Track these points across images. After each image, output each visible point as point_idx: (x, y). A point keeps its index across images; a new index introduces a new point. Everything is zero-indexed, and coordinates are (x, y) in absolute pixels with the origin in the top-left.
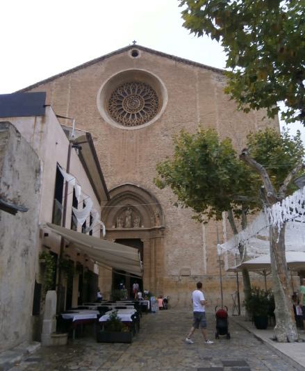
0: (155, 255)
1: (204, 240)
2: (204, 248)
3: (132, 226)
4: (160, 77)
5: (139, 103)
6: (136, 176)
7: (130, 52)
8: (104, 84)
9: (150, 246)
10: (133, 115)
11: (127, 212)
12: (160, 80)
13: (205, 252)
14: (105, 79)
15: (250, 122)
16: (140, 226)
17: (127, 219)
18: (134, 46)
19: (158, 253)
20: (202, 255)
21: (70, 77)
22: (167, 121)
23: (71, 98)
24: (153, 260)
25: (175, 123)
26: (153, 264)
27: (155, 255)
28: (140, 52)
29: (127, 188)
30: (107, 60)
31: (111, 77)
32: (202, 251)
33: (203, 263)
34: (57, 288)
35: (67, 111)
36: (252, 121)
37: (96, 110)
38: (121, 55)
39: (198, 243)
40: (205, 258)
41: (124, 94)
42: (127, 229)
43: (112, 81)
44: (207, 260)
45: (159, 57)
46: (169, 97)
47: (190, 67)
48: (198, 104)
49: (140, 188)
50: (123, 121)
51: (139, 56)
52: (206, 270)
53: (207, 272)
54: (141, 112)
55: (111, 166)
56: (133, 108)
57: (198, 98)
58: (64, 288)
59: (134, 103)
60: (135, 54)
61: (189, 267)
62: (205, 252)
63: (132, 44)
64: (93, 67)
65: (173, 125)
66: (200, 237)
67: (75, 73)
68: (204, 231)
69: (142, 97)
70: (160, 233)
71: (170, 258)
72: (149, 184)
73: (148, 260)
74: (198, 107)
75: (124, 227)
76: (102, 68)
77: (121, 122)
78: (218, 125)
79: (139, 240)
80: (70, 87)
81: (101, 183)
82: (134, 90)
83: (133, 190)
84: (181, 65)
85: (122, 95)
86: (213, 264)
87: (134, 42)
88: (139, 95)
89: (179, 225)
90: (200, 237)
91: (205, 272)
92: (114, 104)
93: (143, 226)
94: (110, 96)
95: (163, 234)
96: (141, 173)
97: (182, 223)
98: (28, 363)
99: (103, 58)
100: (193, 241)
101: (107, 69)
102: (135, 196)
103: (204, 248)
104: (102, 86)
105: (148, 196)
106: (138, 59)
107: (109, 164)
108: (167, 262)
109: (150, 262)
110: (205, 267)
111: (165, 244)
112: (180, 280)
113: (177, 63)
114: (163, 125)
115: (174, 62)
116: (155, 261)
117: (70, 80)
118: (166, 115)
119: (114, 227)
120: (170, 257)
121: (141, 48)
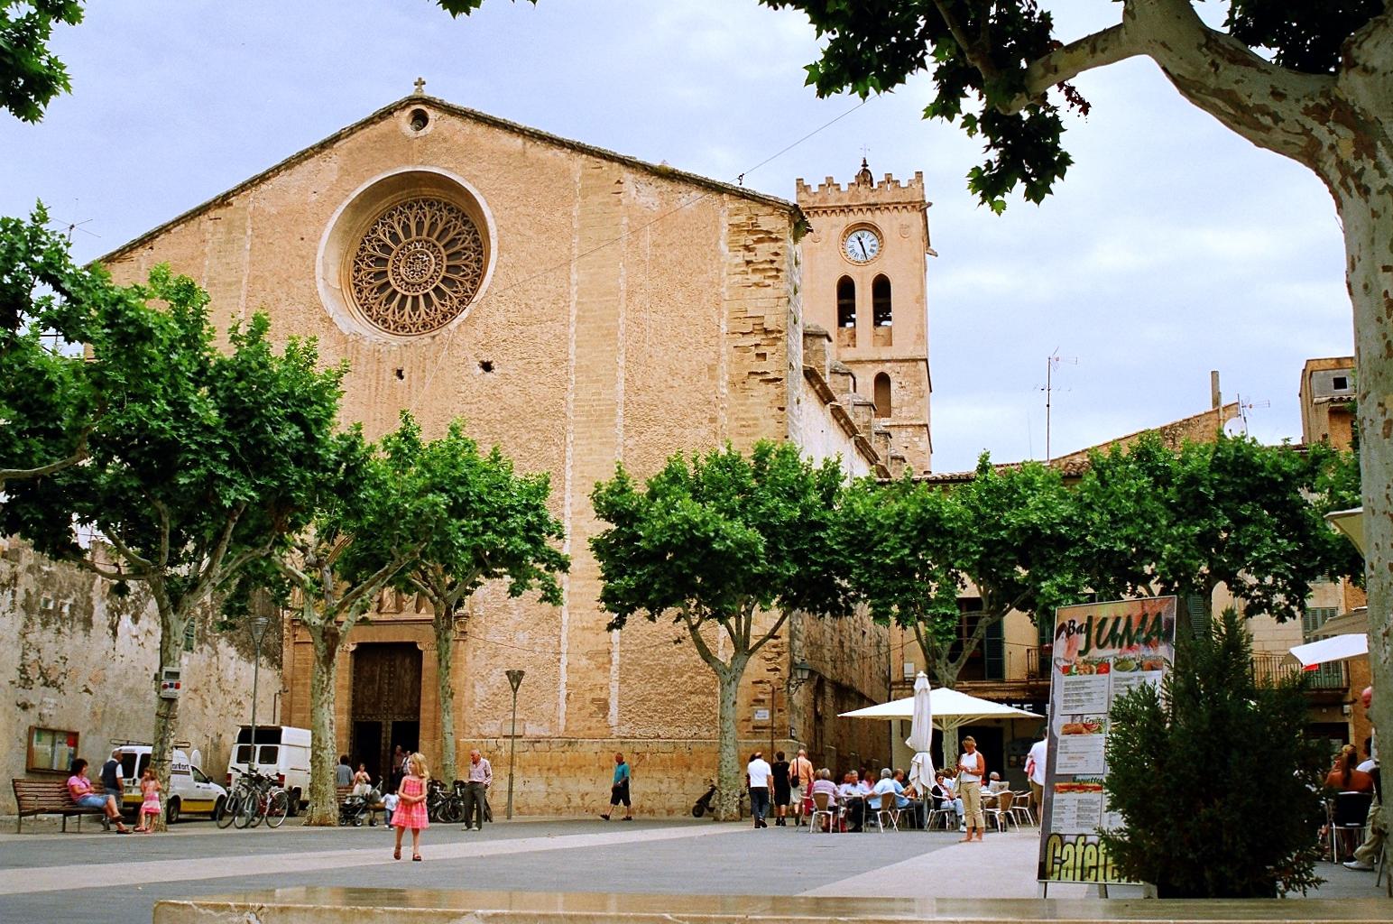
1: (564, 649)
2: (563, 667)
3: (399, 609)
5: (433, 265)
7: (403, 119)
8: (335, 217)
10: (416, 299)
13: (564, 679)
14: (336, 204)
15: (708, 319)
16: (418, 611)
20: (556, 684)
22: (490, 322)
23: (252, 263)
25: (511, 325)
28: (432, 114)
31: (354, 195)
34: (1374, 752)
35: (242, 303)
36: (713, 311)
38: (383, 126)
40: (564, 692)
41: (385, 248)
42: (389, 617)
47: (562, 154)
48: (573, 269)
50: (390, 318)
51: (429, 128)
52: (562, 722)
54: (437, 289)
56: (417, 279)
58: (1375, 747)
59: (418, 267)
63: (410, 91)
64: (309, 165)
65: (505, 334)
66: (554, 641)
67: (263, 187)
68: (565, 622)
72: (130, 617)
74: (574, 277)
75: (378, 611)
76: (330, 165)
77: (385, 321)
78: (622, 328)
82: (406, 229)
84: (539, 151)
85: (388, 242)
87: (420, 83)
88: (433, 239)
90: (554, 641)
91: (562, 728)
92: (369, 269)
93: (423, 611)
94: (357, 248)
101: (344, 171)
103: (563, 667)
104: (331, 224)
106: (425, 139)
108: (472, 704)
112: (499, 747)
113: (529, 144)
115: (519, 142)
118: (488, 305)
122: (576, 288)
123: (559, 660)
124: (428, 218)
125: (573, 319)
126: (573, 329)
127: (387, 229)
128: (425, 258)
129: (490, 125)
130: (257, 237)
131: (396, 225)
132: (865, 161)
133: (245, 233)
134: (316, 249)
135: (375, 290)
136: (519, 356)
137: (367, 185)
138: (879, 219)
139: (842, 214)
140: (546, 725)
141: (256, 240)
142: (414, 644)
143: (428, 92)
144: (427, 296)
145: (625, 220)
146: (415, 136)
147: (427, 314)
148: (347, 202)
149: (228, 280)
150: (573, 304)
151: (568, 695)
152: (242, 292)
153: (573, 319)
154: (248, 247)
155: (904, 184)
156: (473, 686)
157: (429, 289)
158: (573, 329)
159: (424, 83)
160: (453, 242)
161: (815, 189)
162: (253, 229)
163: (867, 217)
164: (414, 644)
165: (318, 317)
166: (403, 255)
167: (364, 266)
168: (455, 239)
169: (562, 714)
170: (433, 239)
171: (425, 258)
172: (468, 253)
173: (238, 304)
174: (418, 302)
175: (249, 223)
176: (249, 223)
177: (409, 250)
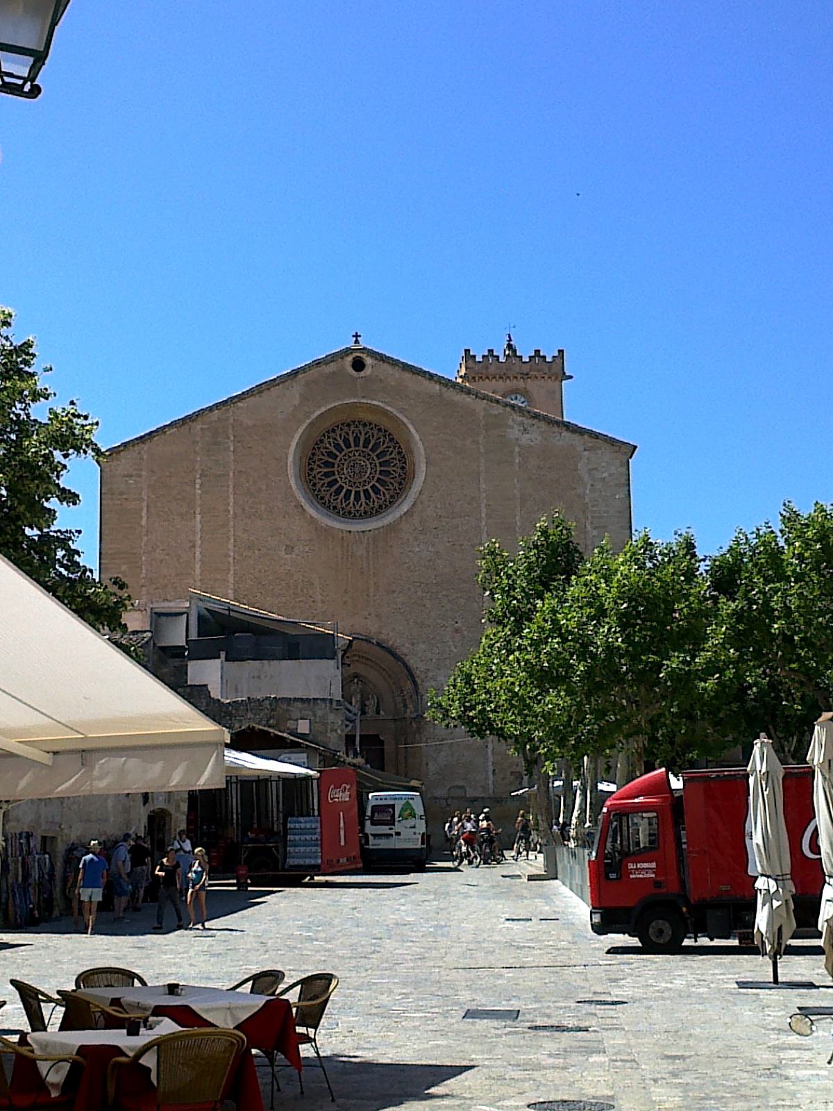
8: (301, 431)
13: (491, 759)
14: (300, 422)
28: (368, 361)
33: (487, 778)
38: (332, 367)
40: (491, 768)
50: (339, 506)
51: (367, 371)
52: (491, 786)
53: (493, 792)
57: (482, 468)
60: (358, 365)
62: (491, 759)
69: (373, 455)
71: (432, 767)
76: (295, 390)
91: (491, 791)
101: (304, 398)
113: (444, 389)
122: (484, 495)
123: (487, 746)
124: (363, 434)
125: (483, 515)
126: (483, 523)
127: (331, 440)
128: (363, 463)
129: (414, 373)
130: (238, 442)
131: (338, 438)
132: (510, 337)
133: (229, 438)
134: (287, 454)
135: (367, 501)
136: (446, 539)
137: (323, 409)
138: (531, 385)
139: (501, 380)
140: (480, 789)
141: (239, 444)
142: (377, 736)
143: (363, 343)
144: (366, 491)
145: (517, 449)
146: (358, 376)
147: (367, 504)
148: (308, 421)
149: (219, 473)
150: (483, 505)
151: (494, 770)
152: (230, 483)
153: (483, 515)
154: (232, 449)
155: (549, 359)
156: (427, 764)
157: (368, 487)
158: (483, 523)
159: (360, 336)
160: (383, 453)
161: (479, 359)
162: (235, 436)
163: (521, 384)
164: (377, 736)
165: (293, 504)
166: (346, 460)
167: (388, 496)
168: (384, 451)
169: (490, 782)
170: (361, 448)
171: (363, 463)
172: (395, 462)
173: (228, 491)
174: (360, 495)
175: (230, 431)
176: (230, 431)
177: (354, 455)
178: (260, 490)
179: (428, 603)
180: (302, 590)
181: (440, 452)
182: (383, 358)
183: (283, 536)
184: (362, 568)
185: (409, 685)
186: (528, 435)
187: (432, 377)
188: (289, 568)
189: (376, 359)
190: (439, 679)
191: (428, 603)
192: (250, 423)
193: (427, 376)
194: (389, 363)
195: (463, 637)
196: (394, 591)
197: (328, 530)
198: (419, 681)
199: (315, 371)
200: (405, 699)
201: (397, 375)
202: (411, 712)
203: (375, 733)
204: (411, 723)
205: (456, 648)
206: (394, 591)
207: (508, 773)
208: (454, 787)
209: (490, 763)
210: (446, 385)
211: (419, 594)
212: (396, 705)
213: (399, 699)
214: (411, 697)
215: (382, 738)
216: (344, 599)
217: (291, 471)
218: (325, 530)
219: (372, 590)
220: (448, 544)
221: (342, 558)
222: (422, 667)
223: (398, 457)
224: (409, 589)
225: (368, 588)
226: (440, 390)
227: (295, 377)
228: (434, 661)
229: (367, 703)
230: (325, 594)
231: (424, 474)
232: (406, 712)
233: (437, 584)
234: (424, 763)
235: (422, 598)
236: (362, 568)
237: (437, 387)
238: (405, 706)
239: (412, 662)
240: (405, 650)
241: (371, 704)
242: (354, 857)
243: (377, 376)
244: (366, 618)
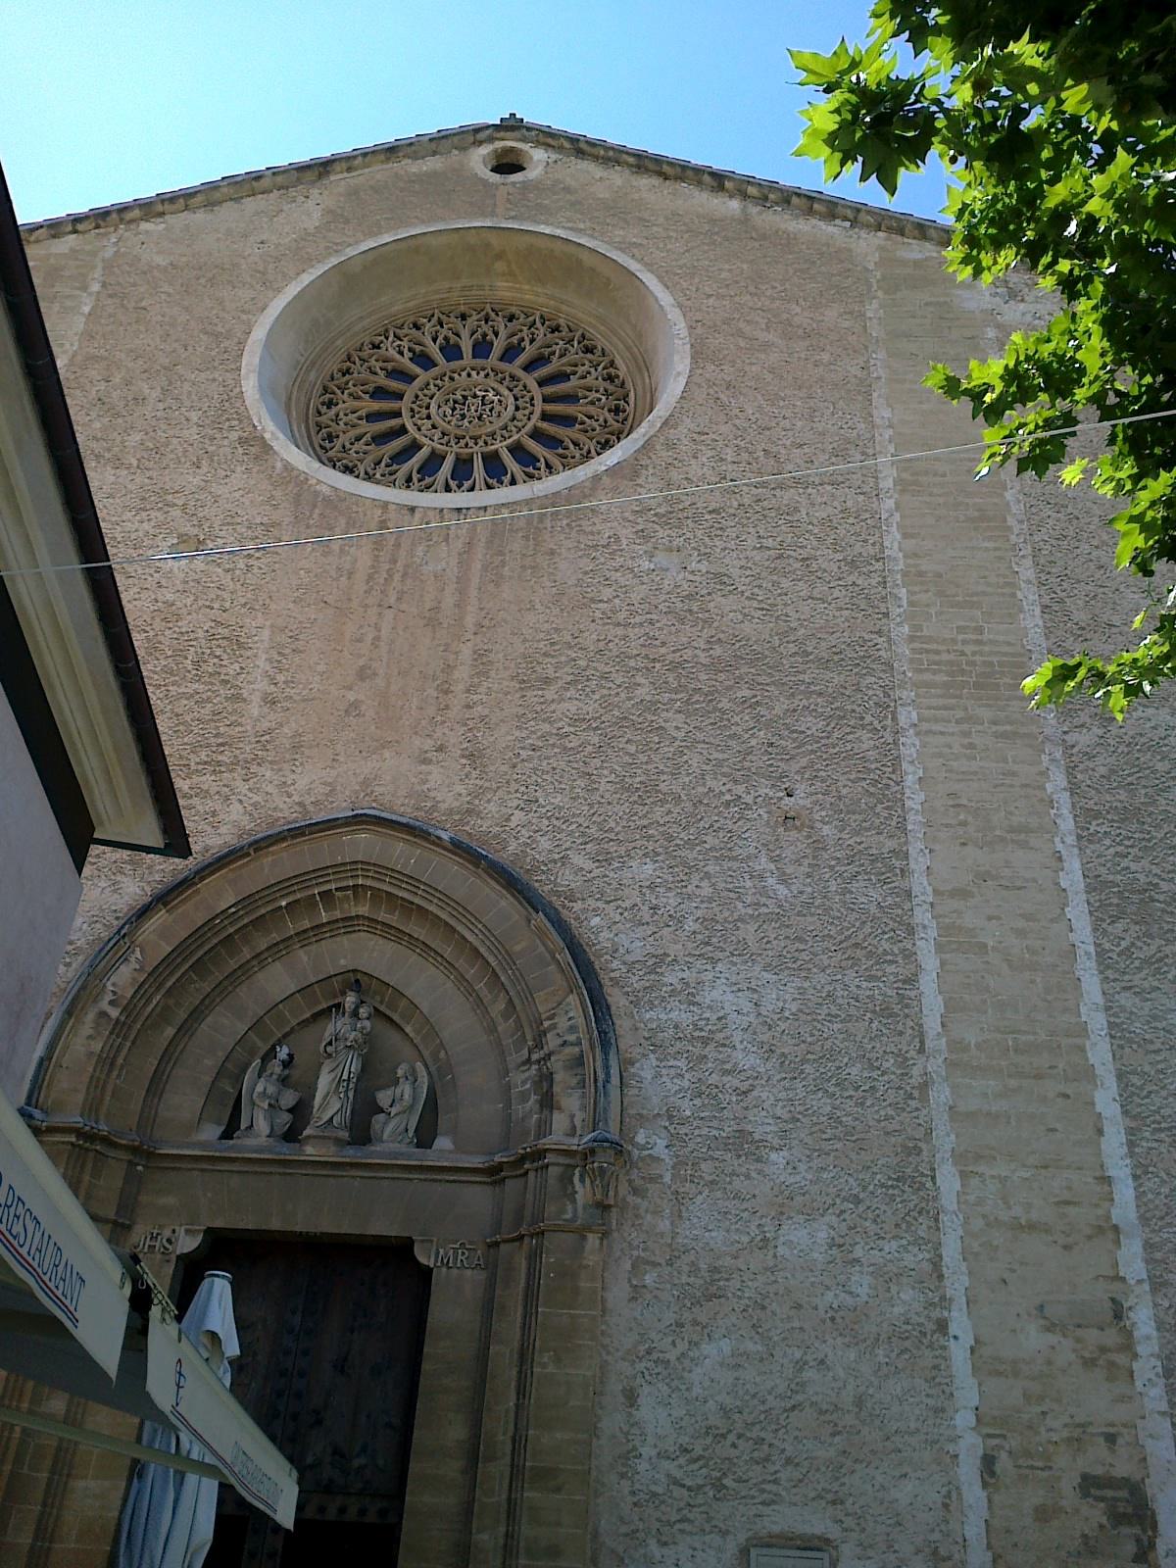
0: (521, 1391)
4: (649, 267)
6: (436, 775)
7: (478, 159)
9: (489, 1308)
11: (339, 1025)
12: (649, 279)
13: (967, 1392)
14: (309, 262)
17: (324, 1082)
18: (512, 125)
19: (545, 1365)
21: (109, 244)
24: (504, 1440)
26: (497, 1471)
27: (521, 1391)
28: (538, 157)
29: (363, 844)
30: (337, 178)
32: (938, 1376)
33: (950, 1500)
37: (232, 396)
39: (907, 1299)
40: (970, 1447)
43: (348, 281)
44: (988, 1462)
45: (645, 182)
46: (698, 355)
47: (833, 231)
49: (458, 848)
51: (532, 173)
55: (270, 701)
60: (508, 165)
61: (817, 1523)
62: (967, 1392)
68: (949, 1199)
69: (530, 380)
70: (583, 1192)
71: (657, 1416)
73: (456, 1432)
74: (882, 413)
76: (311, 208)
79: (399, 1251)
80: (95, 287)
81: (100, 479)
83: (400, 853)
86: (1043, 1514)
89: (743, 1143)
93: (443, 1143)
95: (604, 1208)
96: (473, 757)
97: (763, 1127)
98: (814, 1454)
99: (321, 168)
100: (862, 1285)
101: (333, 217)
102: (409, 909)
105: (506, 903)
106: (526, 186)
107: (256, 687)
108: (630, 1455)
109: (474, 1454)
110: (974, 1530)
111: (617, 1294)
114: (649, 493)
116: (518, 1442)
117: (109, 253)
119: (211, 1132)
120: (648, 1411)
121: (547, 137)
123: (942, 1326)
153: (887, 483)
172: (593, 395)
176: (98, 273)
178: (140, 400)
179: (673, 721)
180: (197, 664)
181: (740, 333)
182: (579, 147)
183: (176, 513)
184: (436, 609)
185: (574, 1011)
186: (1022, 306)
187: (718, 180)
188: (170, 597)
189: (560, 149)
190: (707, 997)
191: (673, 721)
192: (161, 260)
193: (707, 178)
194: (596, 158)
195: (819, 845)
196: (547, 681)
197: (337, 502)
198: (617, 999)
199: (380, 172)
200: (549, 1077)
201: (619, 182)
202: (573, 1131)
203: (392, 1230)
204: (566, 1180)
205: (784, 880)
206: (547, 681)
207: (1068, 1485)
208: (771, 1542)
209: (964, 1419)
210: (763, 200)
211: (642, 692)
212: (508, 1105)
213: (522, 1080)
214: (579, 1061)
215: (422, 1260)
216: (351, 696)
217: (252, 358)
218: (327, 501)
219: (462, 674)
220: (757, 556)
221: (370, 577)
222: (635, 944)
223: (602, 385)
224: (605, 676)
225: (449, 668)
226: (744, 210)
227: (320, 176)
228: (690, 925)
229: (383, 1098)
230: (281, 678)
231: (683, 381)
232: (544, 1128)
233: (715, 667)
234: (615, 1386)
235: (652, 707)
236: (436, 609)
237: (735, 205)
238: (548, 1102)
239: (597, 926)
240: (567, 878)
241: (402, 1100)
242: (707, 1419)
243: (557, 181)
244: (426, 761)
